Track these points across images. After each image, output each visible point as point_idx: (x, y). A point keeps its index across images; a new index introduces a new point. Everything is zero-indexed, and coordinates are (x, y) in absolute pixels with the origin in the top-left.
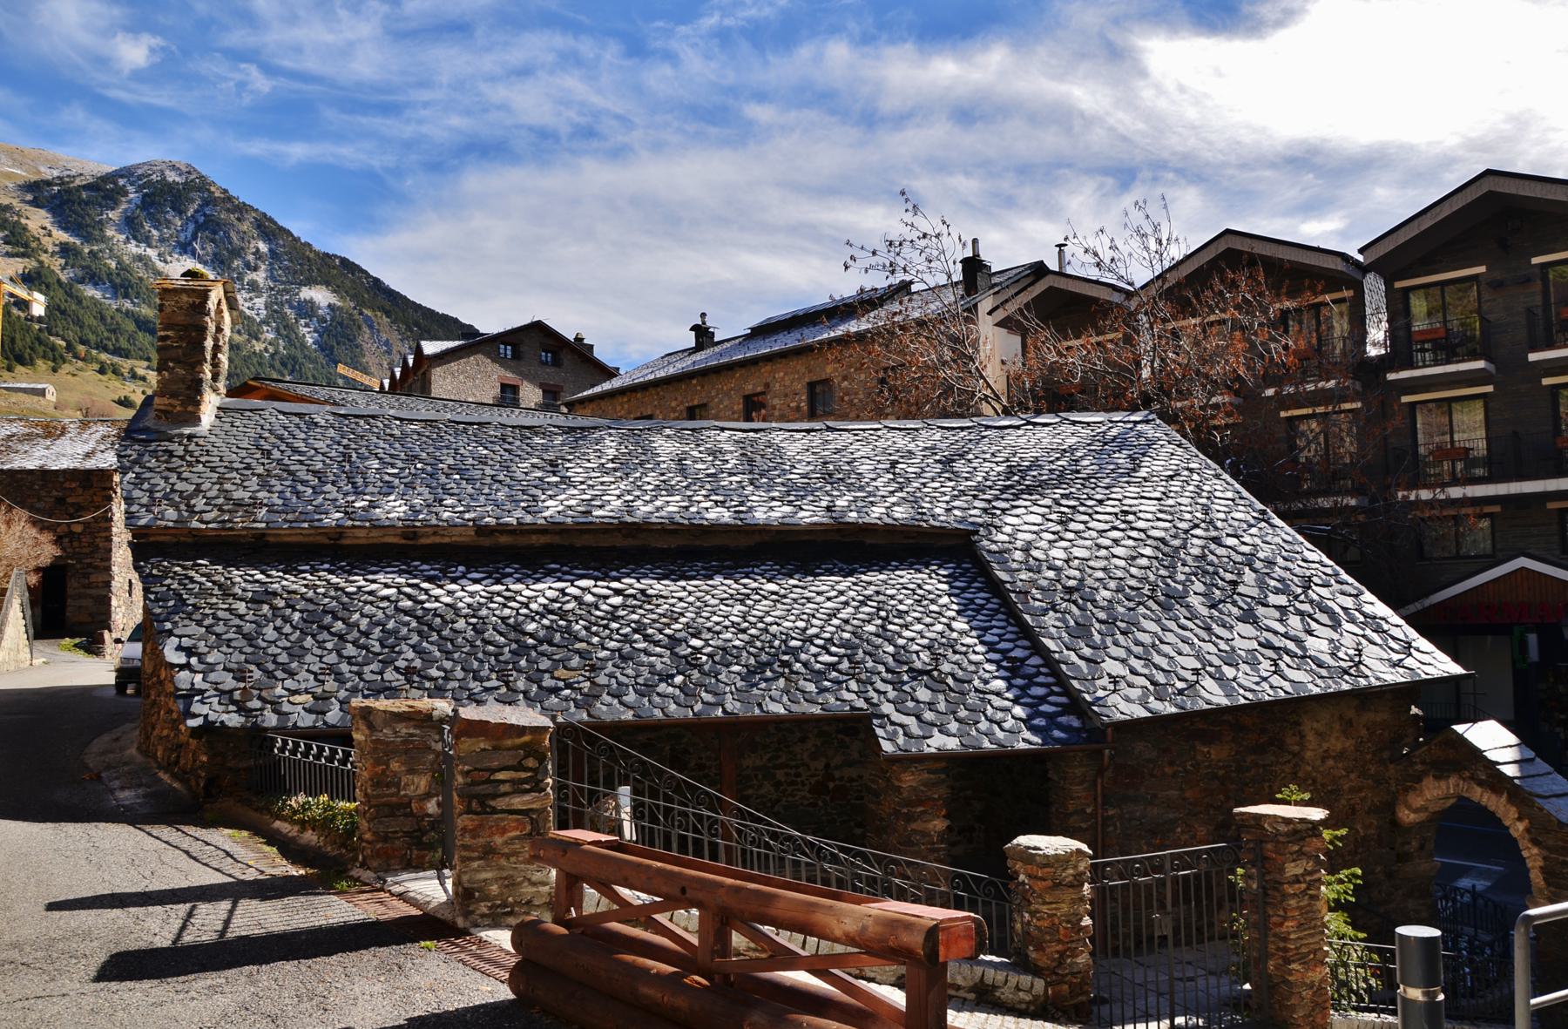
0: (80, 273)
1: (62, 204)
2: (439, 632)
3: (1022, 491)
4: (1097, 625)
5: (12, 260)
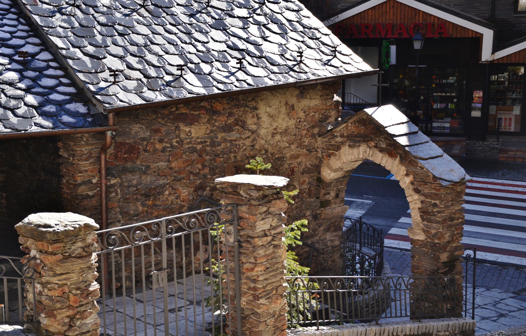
4: (99, 28)
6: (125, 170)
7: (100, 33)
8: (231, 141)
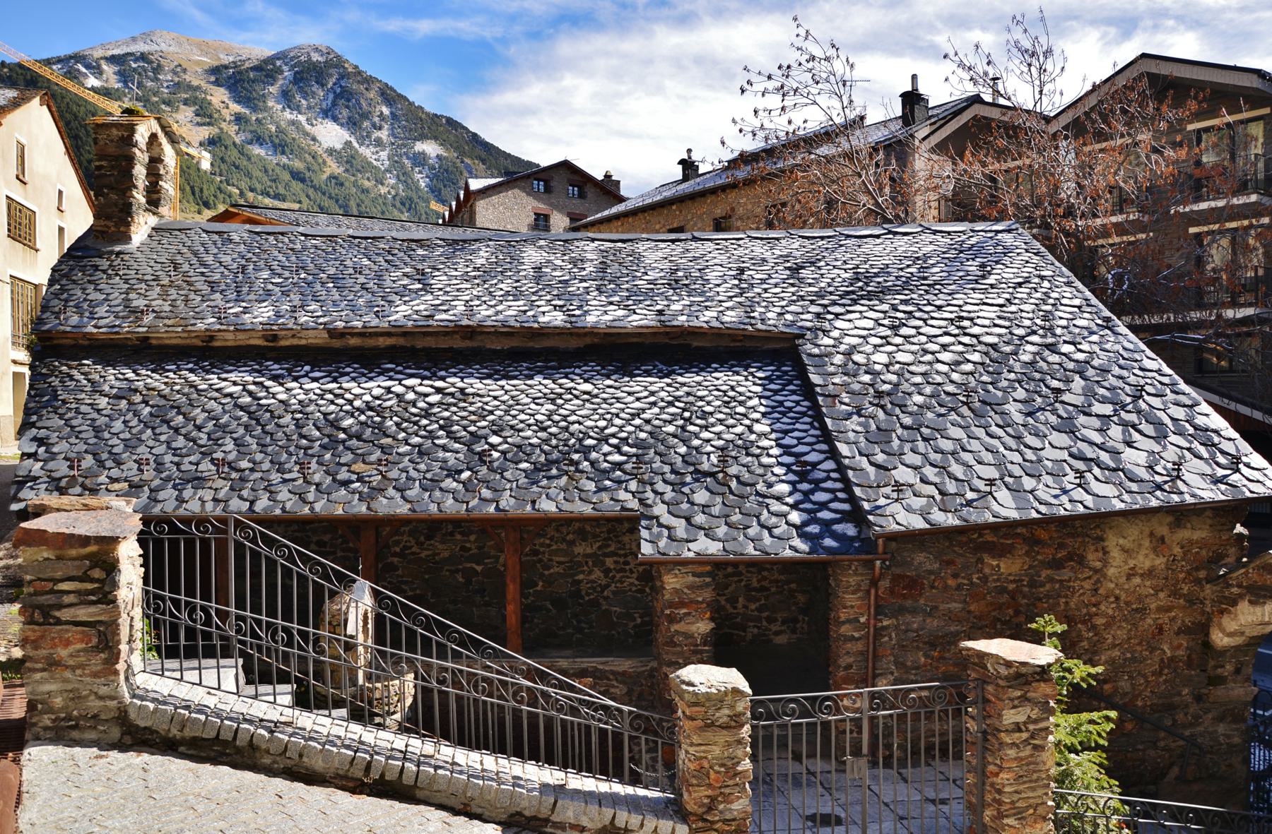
0: (250, 136)
2: (263, 426)
3: (862, 297)
4: (900, 431)
5: (201, 128)
6: (901, 610)
7: (899, 438)
8: (1061, 581)
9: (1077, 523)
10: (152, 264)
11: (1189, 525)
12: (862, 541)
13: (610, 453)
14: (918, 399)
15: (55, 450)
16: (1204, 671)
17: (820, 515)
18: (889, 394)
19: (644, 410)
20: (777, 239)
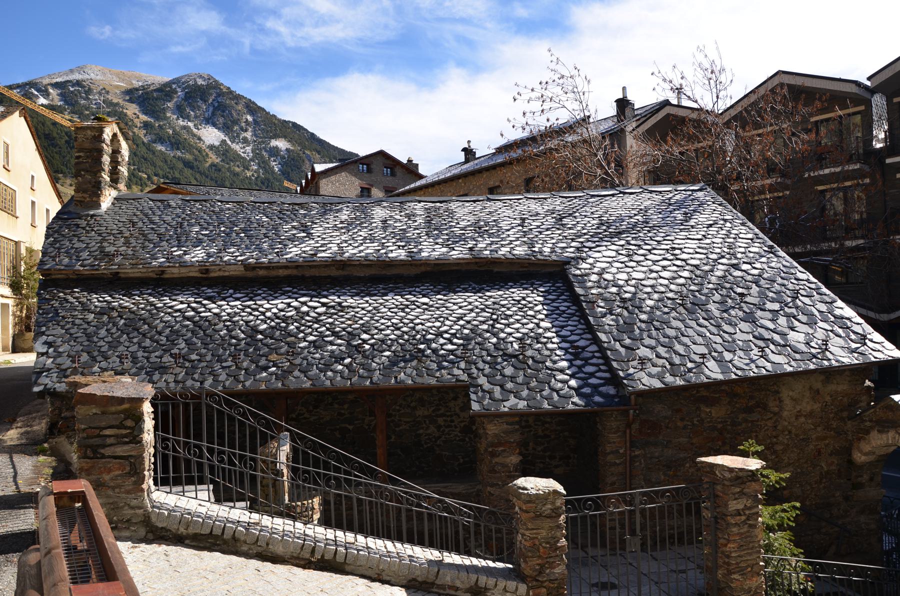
0: (154, 137)
1: (144, 100)
2: (204, 331)
3: (606, 236)
7: (638, 328)
8: (752, 421)
9: (762, 382)
10: (116, 222)
11: (835, 381)
12: (620, 397)
13: (445, 344)
14: (650, 303)
15: (61, 350)
16: (849, 480)
17: (590, 381)
18: (630, 300)
19: (465, 315)
20: (545, 199)
